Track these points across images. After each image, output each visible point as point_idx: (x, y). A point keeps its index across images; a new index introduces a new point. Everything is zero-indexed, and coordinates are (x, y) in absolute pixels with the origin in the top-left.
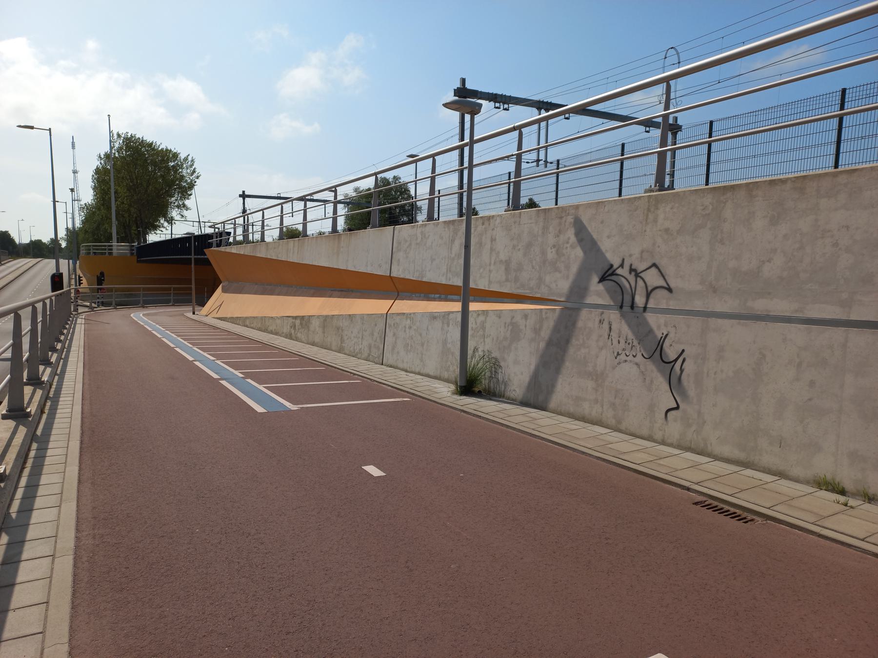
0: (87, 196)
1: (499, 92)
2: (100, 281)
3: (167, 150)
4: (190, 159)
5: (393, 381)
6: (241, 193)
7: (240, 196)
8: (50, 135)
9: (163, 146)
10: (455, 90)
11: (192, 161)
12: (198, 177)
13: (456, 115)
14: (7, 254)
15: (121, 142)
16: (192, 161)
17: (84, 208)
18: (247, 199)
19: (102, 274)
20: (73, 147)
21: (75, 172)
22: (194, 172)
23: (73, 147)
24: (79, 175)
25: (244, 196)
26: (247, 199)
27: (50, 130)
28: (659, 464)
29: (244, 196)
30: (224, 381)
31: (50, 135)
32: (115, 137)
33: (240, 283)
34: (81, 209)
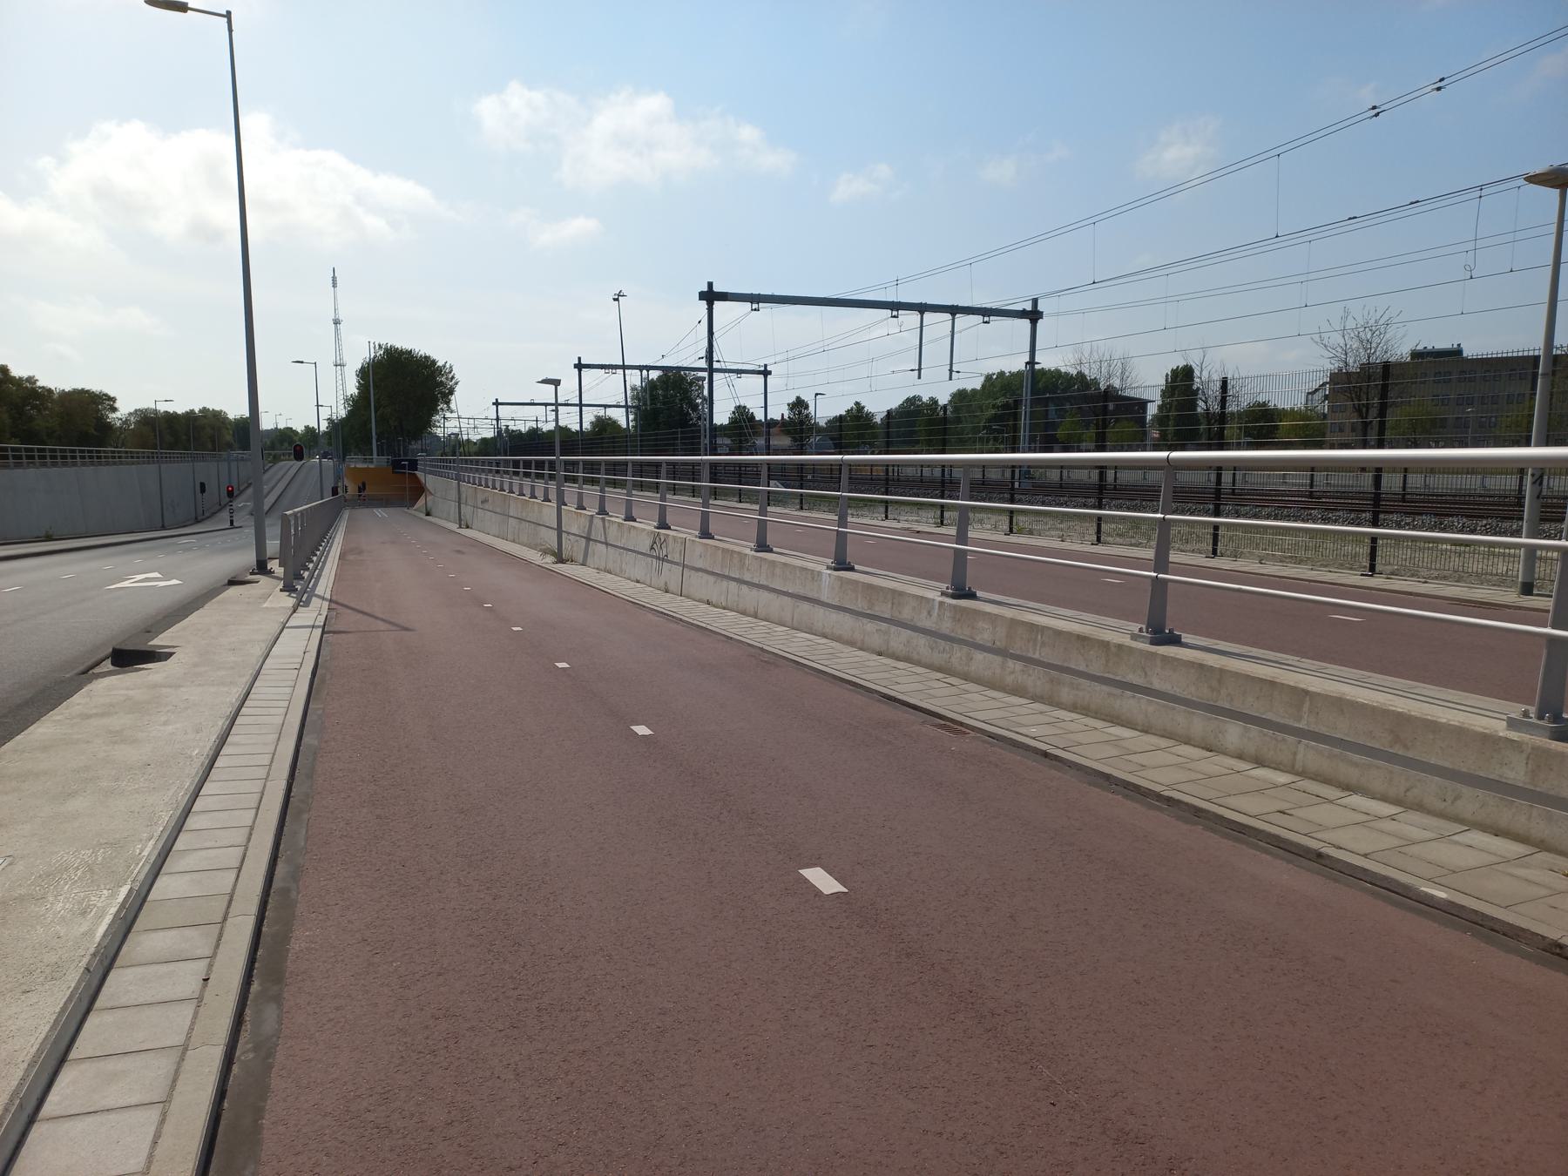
0: (352, 388)
1: (755, 292)
2: (362, 488)
3: (426, 357)
4: (448, 366)
5: (853, 672)
6: (705, 289)
7: (494, 404)
8: (230, 30)
9: (422, 353)
10: (700, 293)
11: (451, 367)
12: (456, 383)
13: (495, 406)
14: (292, 457)
15: (382, 353)
16: (451, 367)
17: (349, 400)
18: (500, 407)
19: (364, 484)
20: (334, 285)
21: (337, 322)
22: (453, 378)
23: (334, 285)
24: (341, 327)
25: (710, 296)
26: (500, 407)
27: (228, 15)
28: (1127, 760)
29: (497, 404)
30: (827, 891)
31: (230, 30)
32: (377, 347)
33: (25, 428)
34: (346, 400)
